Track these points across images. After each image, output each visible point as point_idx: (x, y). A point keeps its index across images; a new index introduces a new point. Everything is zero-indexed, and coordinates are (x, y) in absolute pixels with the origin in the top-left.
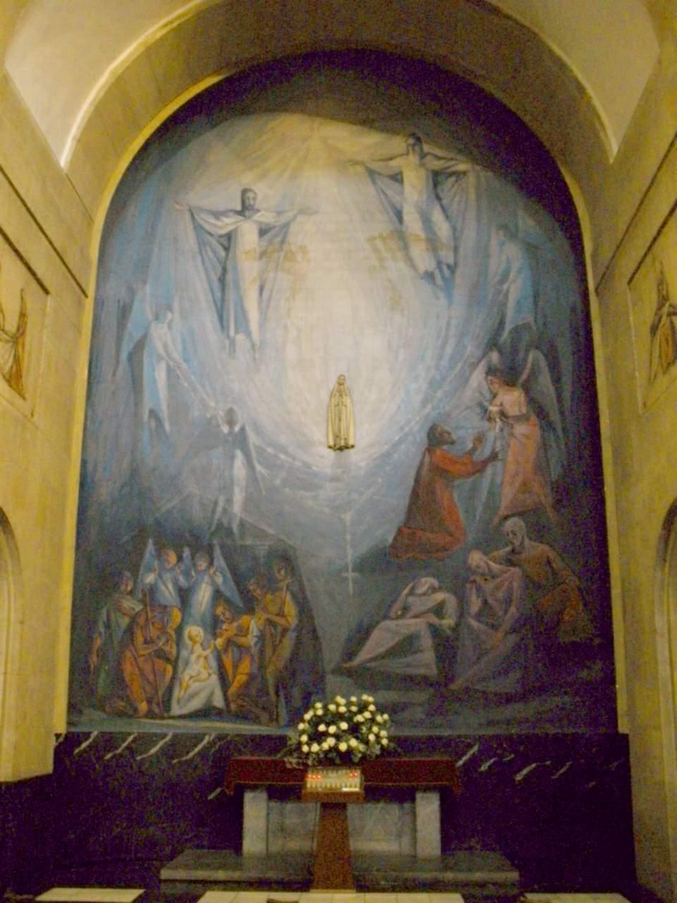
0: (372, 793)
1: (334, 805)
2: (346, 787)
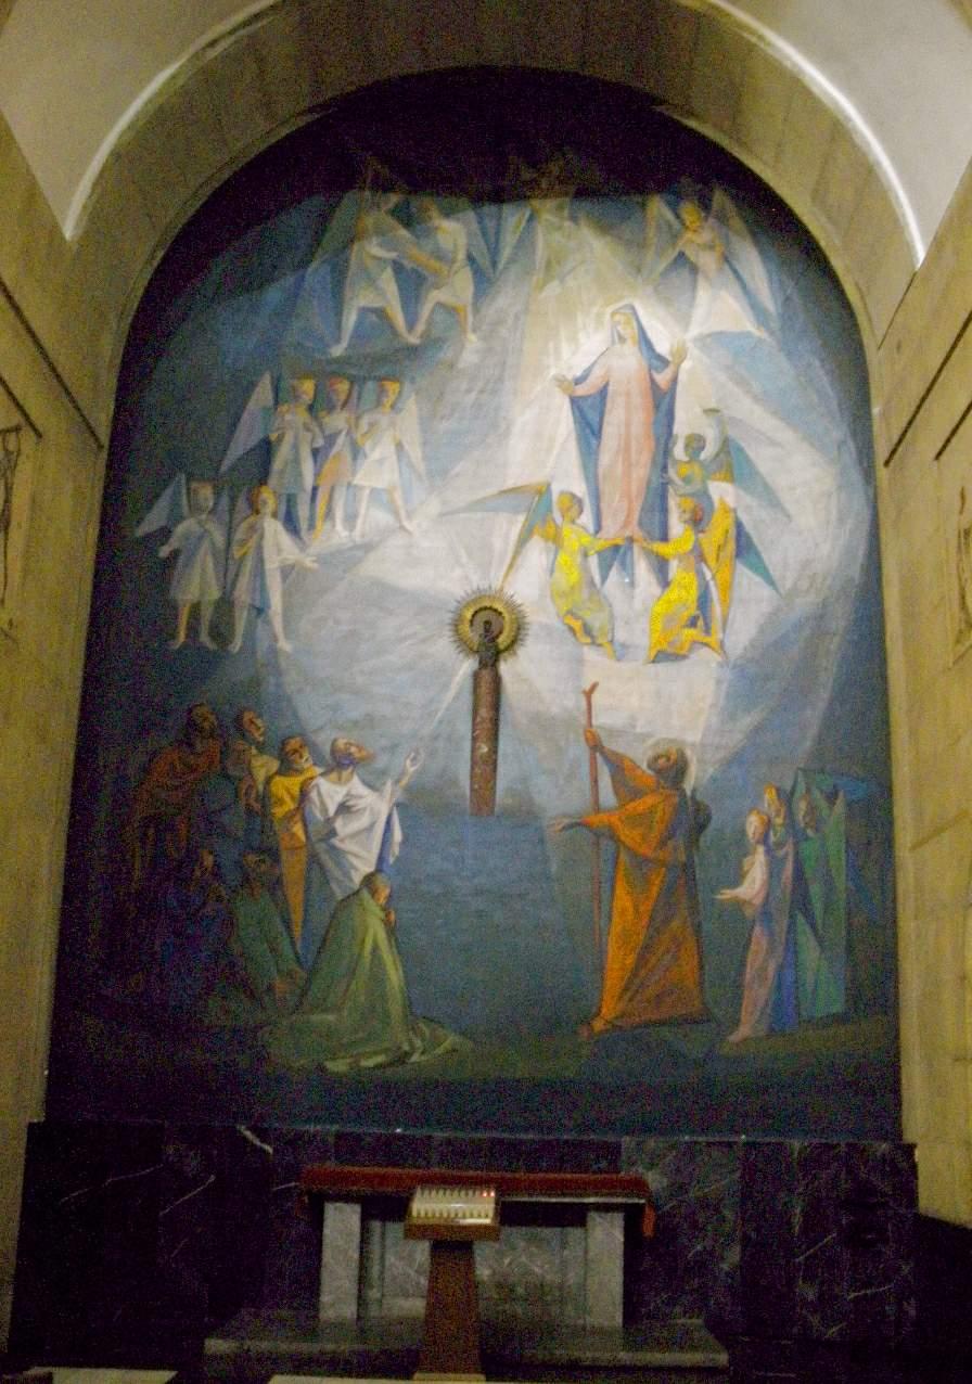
0: (509, 1214)
1: (452, 1245)
2: (472, 1216)
